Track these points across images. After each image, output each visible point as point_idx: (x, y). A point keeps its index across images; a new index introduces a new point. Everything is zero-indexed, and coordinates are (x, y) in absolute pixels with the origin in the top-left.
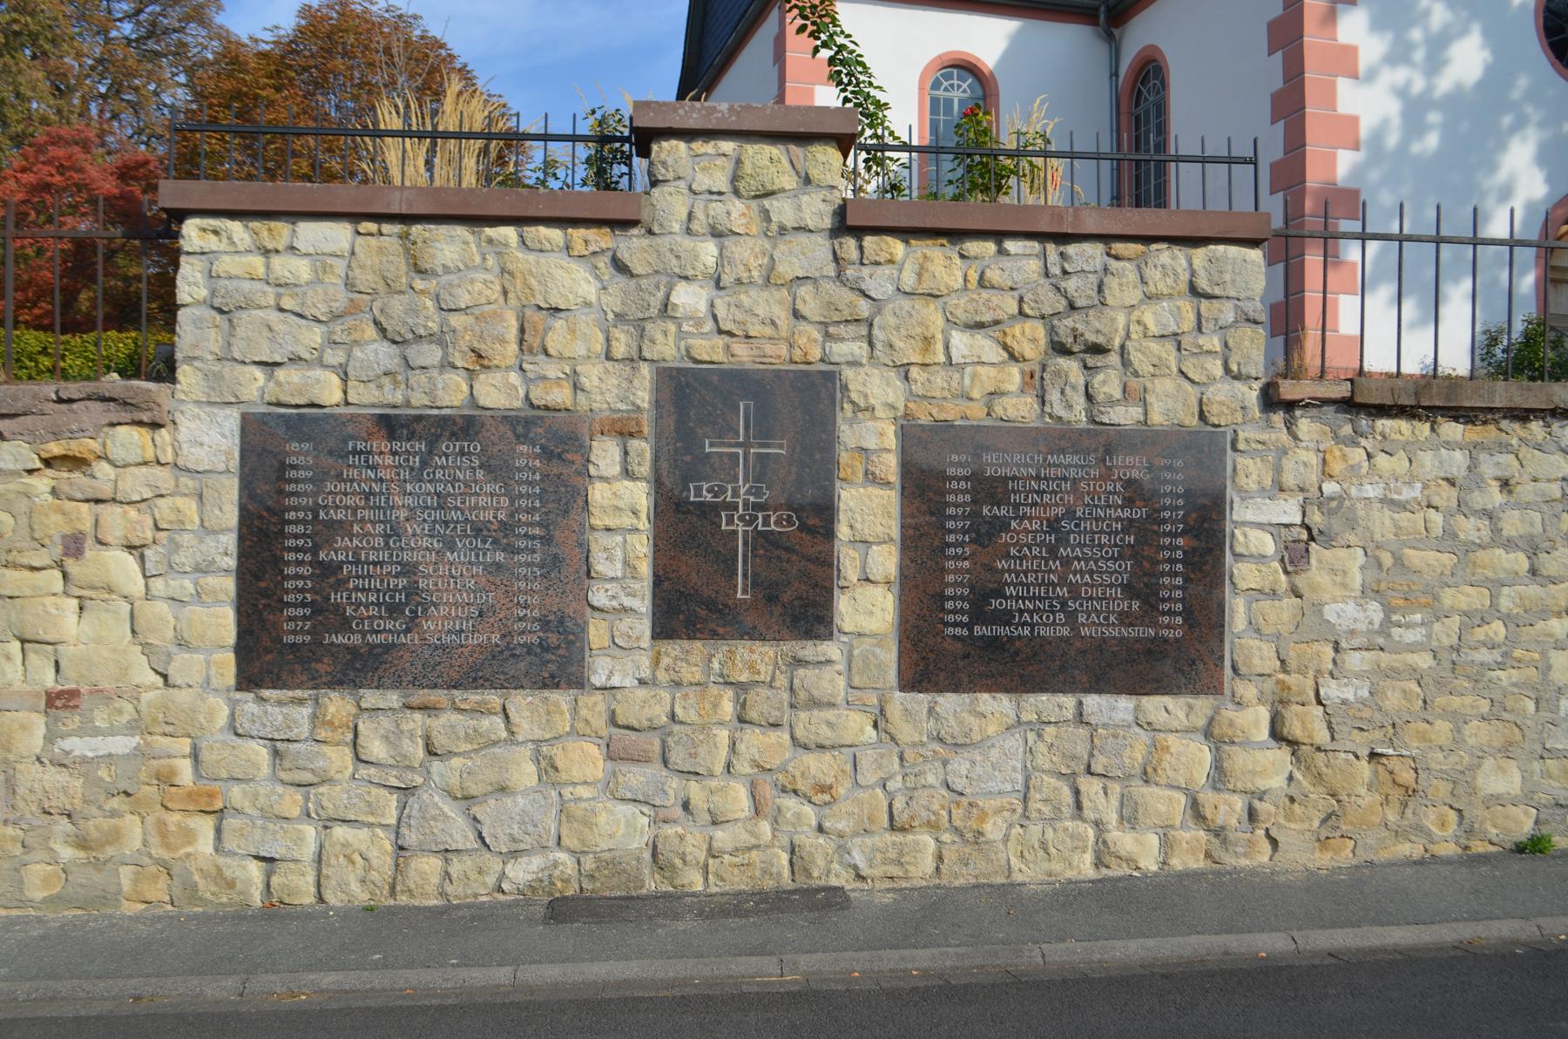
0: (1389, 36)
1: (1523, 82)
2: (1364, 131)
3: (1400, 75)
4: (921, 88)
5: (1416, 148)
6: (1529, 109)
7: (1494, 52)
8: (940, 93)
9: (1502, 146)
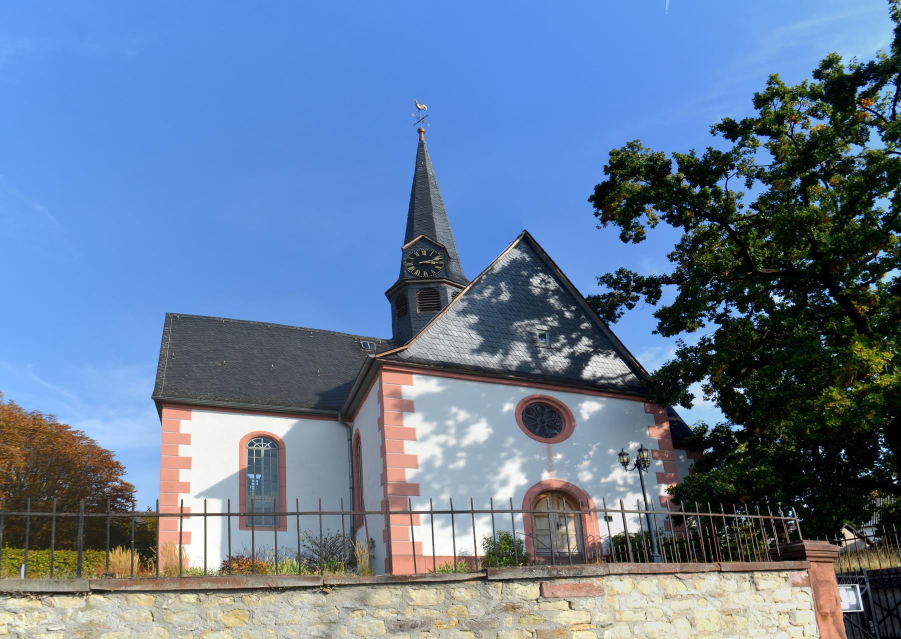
0: (435, 424)
1: (511, 440)
2: (420, 460)
3: (442, 438)
4: (241, 446)
5: (451, 466)
6: (515, 451)
7: (494, 429)
8: (254, 448)
9: (501, 464)
